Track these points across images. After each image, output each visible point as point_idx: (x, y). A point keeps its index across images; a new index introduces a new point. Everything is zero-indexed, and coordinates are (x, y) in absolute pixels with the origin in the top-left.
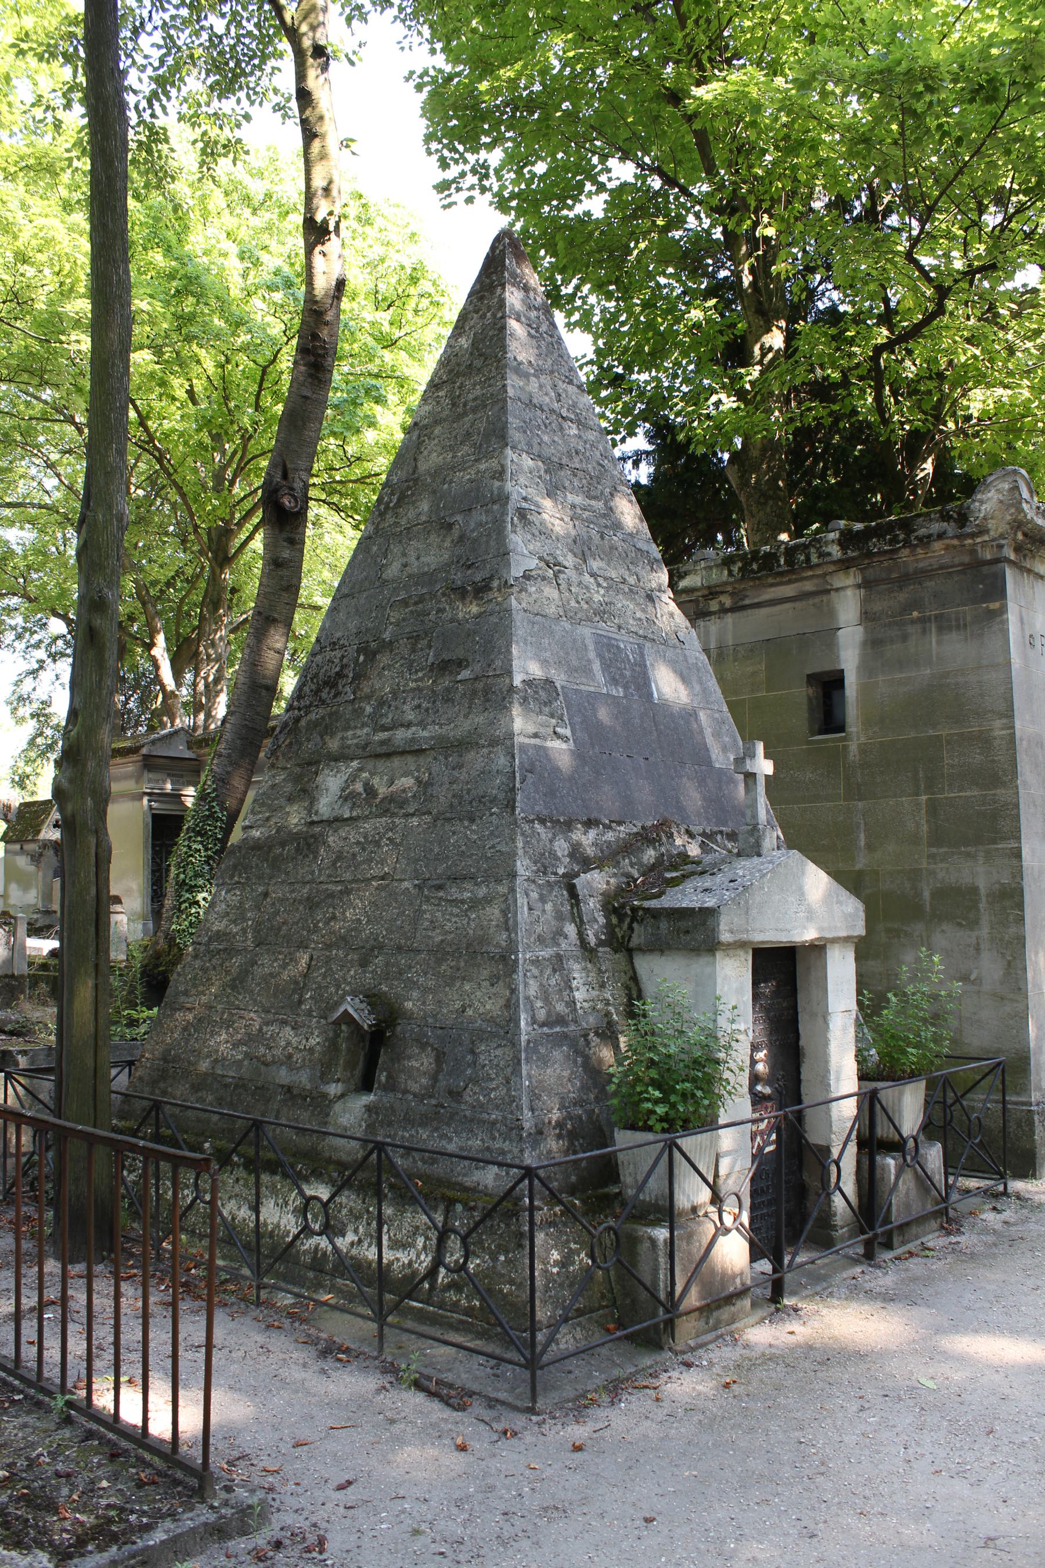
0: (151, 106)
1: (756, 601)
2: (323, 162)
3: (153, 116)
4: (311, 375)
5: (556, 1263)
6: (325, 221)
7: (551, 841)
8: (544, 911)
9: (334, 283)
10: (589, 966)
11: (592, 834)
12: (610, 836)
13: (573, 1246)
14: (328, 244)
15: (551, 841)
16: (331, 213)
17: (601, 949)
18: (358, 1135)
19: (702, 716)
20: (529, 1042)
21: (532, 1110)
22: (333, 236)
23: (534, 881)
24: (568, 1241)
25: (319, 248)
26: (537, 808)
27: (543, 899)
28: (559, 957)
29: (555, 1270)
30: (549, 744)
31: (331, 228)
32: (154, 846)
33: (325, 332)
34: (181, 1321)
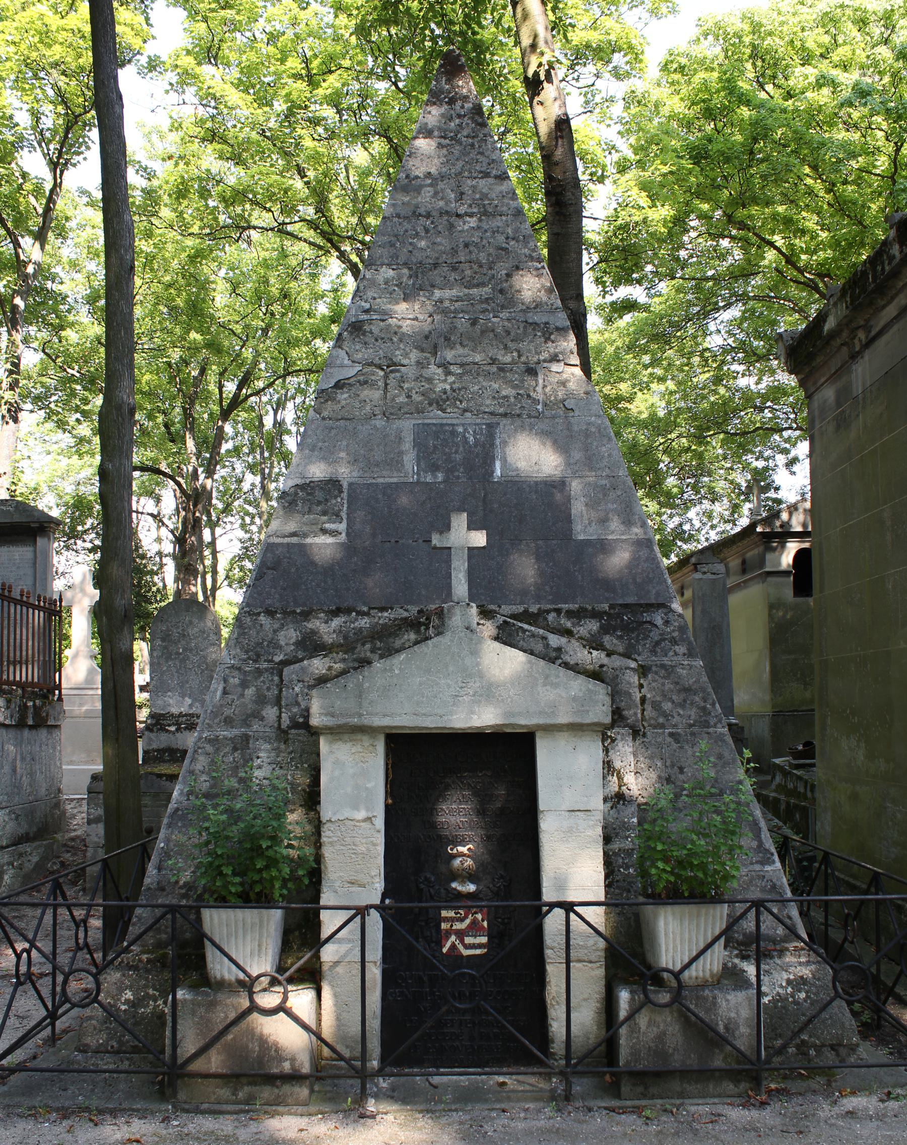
0: (469, 26)
1: (877, 329)
2: (527, 23)
3: (474, 33)
4: (557, 213)
5: (127, 1002)
6: (536, 74)
7: (275, 631)
8: (242, 695)
9: (553, 126)
10: (283, 746)
11: (336, 622)
12: (364, 623)
13: (151, 992)
14: (542, 93)
15: (275, 631)
16: (540, 65)
17: (293, 731)
18: (763, 927)
19: (575, 486)
20: (177, 810)
21: (159, 869)
22: (545, 84)
23: (239, 669)
24: (146, 986)
25: (536, 99)
26: (269, 602)
27: (244, 685)
28: (246, 738)
29: (123, 1007)
30: (309, 540)
31: (542, 77)
32: (771, 650)
33: (558, 171)
34: (179, 1021)
